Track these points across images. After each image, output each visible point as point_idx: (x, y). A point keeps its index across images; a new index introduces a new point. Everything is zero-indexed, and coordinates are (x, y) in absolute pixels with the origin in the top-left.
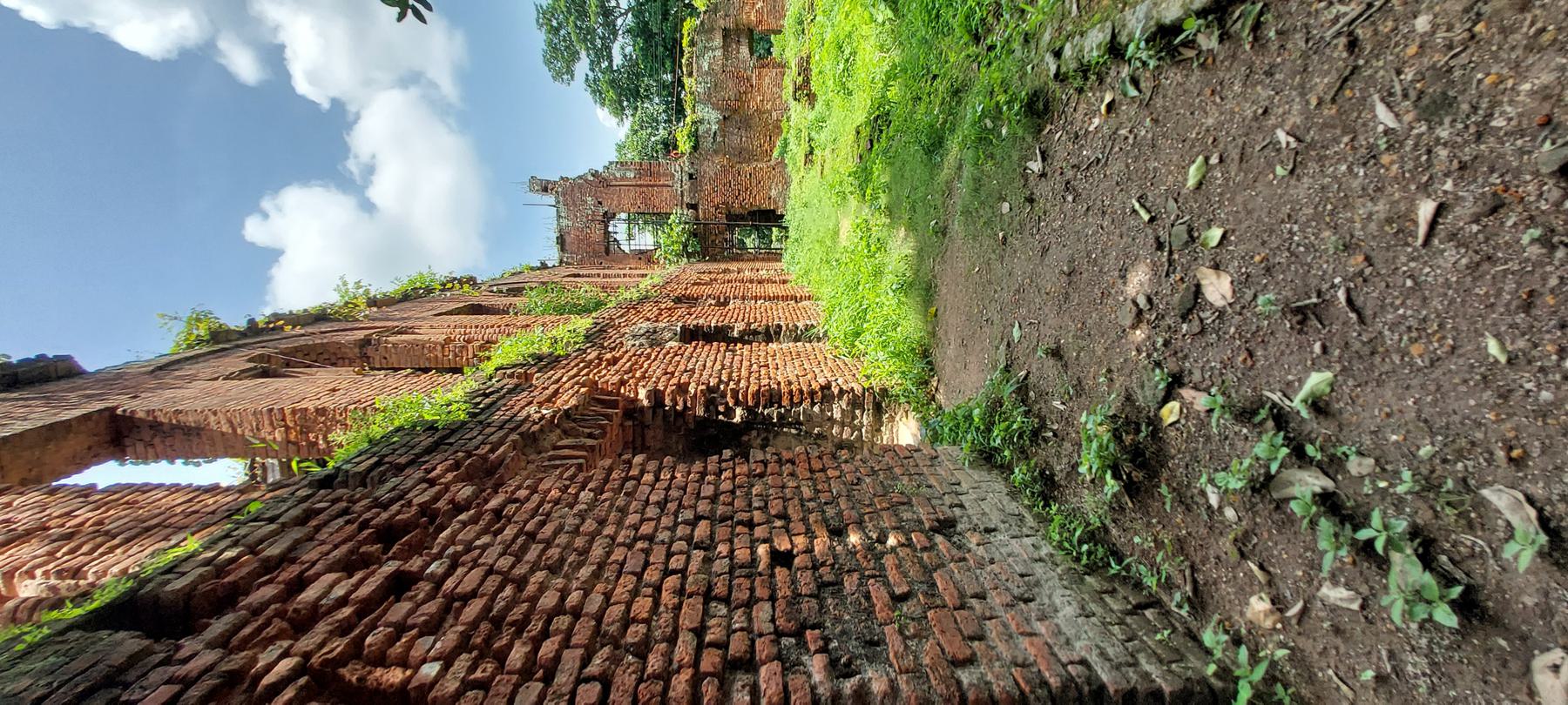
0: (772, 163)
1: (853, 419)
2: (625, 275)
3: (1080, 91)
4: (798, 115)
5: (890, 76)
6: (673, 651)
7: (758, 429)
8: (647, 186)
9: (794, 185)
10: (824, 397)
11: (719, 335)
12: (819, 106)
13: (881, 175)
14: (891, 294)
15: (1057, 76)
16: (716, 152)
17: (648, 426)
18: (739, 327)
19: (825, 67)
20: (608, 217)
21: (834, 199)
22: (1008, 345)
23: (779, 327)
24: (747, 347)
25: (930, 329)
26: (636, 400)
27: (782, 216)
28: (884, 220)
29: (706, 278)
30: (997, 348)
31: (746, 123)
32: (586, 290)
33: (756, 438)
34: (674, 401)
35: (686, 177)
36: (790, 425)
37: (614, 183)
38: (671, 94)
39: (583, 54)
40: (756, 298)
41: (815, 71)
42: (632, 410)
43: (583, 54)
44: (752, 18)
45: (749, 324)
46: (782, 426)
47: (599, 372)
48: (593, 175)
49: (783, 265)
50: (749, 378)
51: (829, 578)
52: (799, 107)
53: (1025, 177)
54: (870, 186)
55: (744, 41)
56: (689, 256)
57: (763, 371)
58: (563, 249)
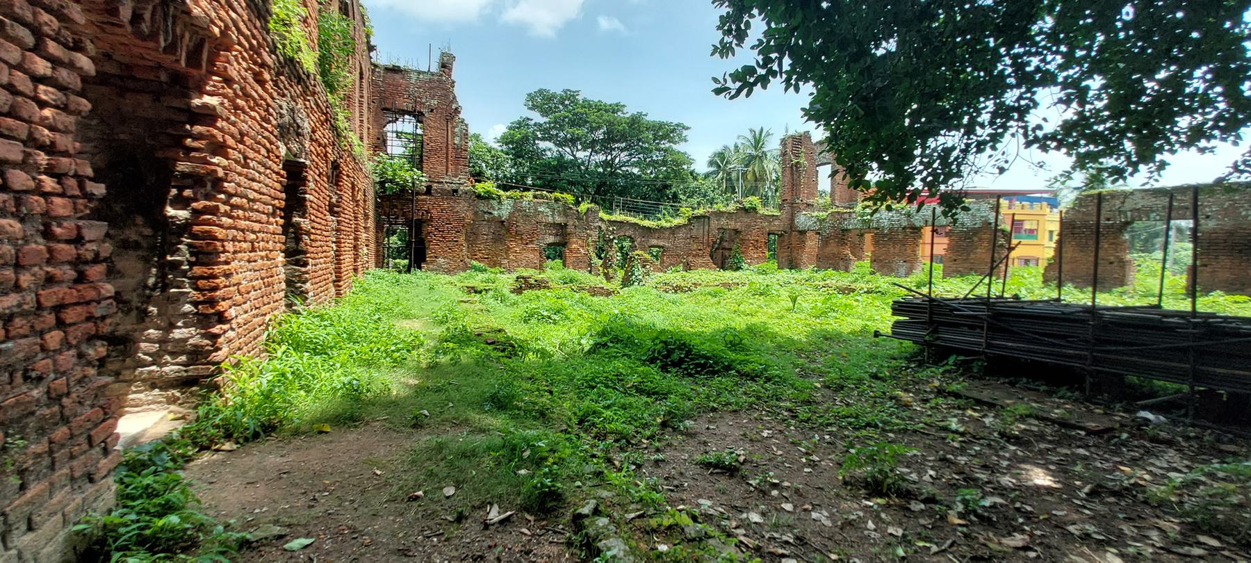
0: (467, 260)
2: (362, 121)
3: (569, 544)
4: (506, 281)
5: (543, 353)
7: (154, 236)
8: (447, 154)
9: (448, 278)
10: (207, 316)
11: (294, 200)
12: (514, 297)
13: (469, 354)
14: (346, 380)
15: (581, 516)
16: (476, 213)
17: (158, 100)
18: (305, 223)
19: (543, 301)
20: (418, 116)
21: (440, 314)
22: (280, 537)
23: (305, 264)
24: (280, 230)
25: (303, 428)
26: (202, 92)
27: (420, 268)
28: (424, 362)
29: (360, 196)
30: (276, 522)
31: (498, 239)
32: (348, 78)
33: (141, 234)
34: (196, 138)
35: (454, 187)
36: (162, 276)
37: (450, 126)
38: (517, 182)
39: (546, 119)
40: (338, 242)
41: (539, 293)
42: (185, 84)
43: (546, 119)
44: (574, 246)
45: (308, 233)
47: (243, 58)
48: (456, 109)
49: (373, 270)
50: (235, 228)
51: (50, 319)
52: (511, 281)
53: (482, 506)
54: (456, 346)
55: (558, 239)
56: (382, 183)
57: (244, 245)
58: (387, 69)
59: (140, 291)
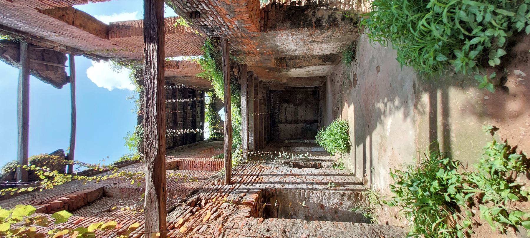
36: (323, 5)
46: (320, 6)
59: (328, 11)
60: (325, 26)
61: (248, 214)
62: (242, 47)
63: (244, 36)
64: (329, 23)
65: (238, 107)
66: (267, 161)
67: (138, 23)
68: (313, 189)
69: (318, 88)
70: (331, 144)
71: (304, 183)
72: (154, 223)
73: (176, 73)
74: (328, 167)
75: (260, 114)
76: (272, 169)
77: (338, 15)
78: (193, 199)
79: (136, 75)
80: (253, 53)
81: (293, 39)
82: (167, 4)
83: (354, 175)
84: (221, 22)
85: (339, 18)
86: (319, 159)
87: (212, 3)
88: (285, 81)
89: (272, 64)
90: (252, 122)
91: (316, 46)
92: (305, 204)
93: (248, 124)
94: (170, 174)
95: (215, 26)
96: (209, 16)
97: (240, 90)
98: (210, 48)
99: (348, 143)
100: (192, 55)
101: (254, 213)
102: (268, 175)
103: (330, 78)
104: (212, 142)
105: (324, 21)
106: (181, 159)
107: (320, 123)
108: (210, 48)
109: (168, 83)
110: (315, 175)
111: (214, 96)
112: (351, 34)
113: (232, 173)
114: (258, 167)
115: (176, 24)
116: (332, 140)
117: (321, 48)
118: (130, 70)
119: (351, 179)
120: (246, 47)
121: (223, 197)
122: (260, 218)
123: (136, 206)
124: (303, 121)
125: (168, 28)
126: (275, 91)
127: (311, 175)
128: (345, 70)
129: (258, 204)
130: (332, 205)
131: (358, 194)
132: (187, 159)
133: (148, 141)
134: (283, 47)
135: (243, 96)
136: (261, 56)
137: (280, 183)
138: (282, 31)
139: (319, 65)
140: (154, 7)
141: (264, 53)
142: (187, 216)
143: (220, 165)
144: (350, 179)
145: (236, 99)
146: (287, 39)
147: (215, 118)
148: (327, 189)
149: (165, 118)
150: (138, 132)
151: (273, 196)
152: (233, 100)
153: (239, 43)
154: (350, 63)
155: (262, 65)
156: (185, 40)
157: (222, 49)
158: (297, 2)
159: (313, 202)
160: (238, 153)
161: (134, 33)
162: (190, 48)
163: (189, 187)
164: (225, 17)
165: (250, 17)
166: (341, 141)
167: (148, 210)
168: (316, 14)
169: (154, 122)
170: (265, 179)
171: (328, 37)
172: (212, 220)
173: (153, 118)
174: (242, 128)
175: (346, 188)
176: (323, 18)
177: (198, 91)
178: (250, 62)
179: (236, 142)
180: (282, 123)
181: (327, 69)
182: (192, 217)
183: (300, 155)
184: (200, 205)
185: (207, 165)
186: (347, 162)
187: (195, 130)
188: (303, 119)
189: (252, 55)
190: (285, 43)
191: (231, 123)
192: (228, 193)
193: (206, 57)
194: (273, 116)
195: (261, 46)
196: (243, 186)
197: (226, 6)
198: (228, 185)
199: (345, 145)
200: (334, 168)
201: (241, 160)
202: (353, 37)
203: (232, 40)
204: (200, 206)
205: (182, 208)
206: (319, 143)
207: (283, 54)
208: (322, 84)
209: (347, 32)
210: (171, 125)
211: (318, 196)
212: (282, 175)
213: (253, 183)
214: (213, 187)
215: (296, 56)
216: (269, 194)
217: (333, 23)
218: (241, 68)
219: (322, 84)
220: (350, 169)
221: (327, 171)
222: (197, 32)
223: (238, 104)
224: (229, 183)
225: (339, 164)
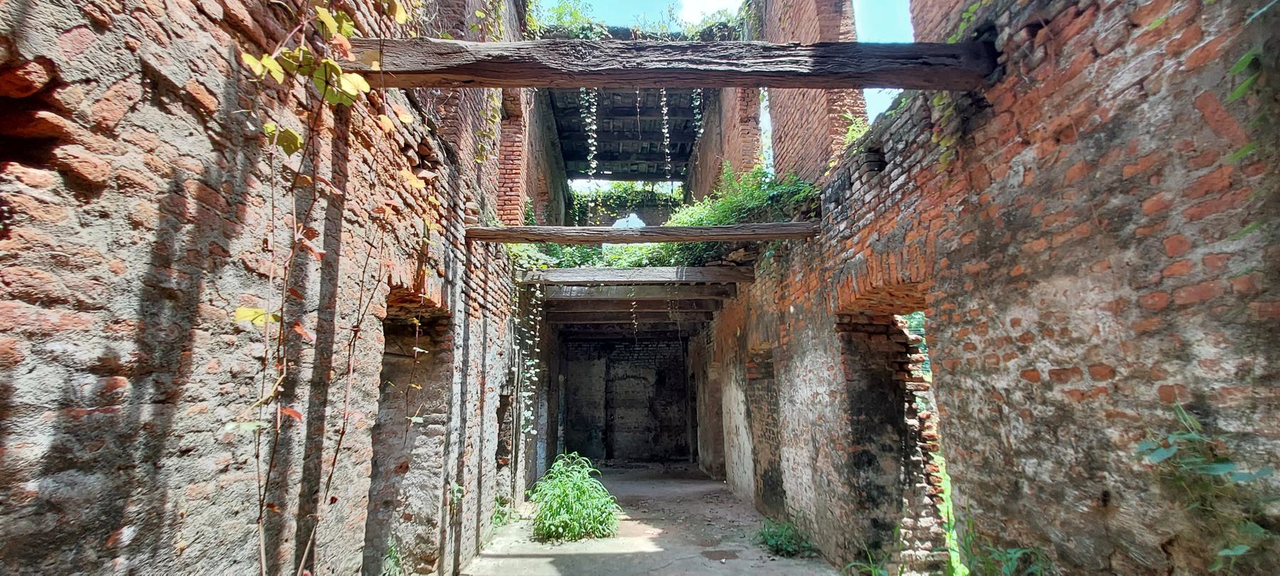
1: (920, 540)
6: (316, 167)
33: (891, 439)
36: (908, 473)
46: (906, 465)
59: (896, 486)
60: (858, 477)
61: (395, 281)
62: (798, 270)
63: (827, 275)
64: (866, 486)
65: (650, 259)
66: (517, 330)
67: (848, 32)
68: (448, 445)
69: (695, 460)
70: (557, 491)
71: (464, 421)
72: (389, 59)
73: (730, 115)
74: (498, 484)
75: (632, 314)
76: (500, 343)
77: (883, 512)
78: (436, 149)
79: (725, 26)
80: (782, 298)
81: (820, 397)
82: (901, 95)
83: (478, 554)
84: (859, 220)
85: (878, 513)
86: (519, 460)
87: (907, 200)
88: (712, 375)
89: (757, 342)
90: (613, 293)
91: (805, 455)
92: (416, 424)
93: (607, 284)
94: (494, 97)
95: (850, 207)
96: (873, 193)
97: (693, 265)
98: (794, 194)
99: (559, 536)
100: (775, 154)
101: (399, 297)
102: (485, 333)
103: (722, 490)
104: (562, 198)
105: (871, 474)
106: (527, 124)
107: (607, 466)
108: (794, 194)
109: (705, 97)
110: (481, 450)
111: (676, 204)
112: (838, 545)
113: (492, 244)
114: (504, 309)
115: (849, 115)
116: (566, 495)
117: (800, 468)
118: (735, 13)
119: (468, 543)
120: (797, 279)
121: (438, 222)
122: (385, 310)
123: (424, 21)
124: (613, 420)
125: (839, 99)
126: (686, 350)
127: (481, 441)
128: (745, 530)
129: (415, 305)
130: (405, 494)
131: (432, 562)
132: (525, 139)
133: (585, 49)
134: (800, 371)
135: (677, 273)
136: (775, 316)
137: (465, 362)
138: (842, 367)
139: (756, 461)
140: (897, 65)
141: (783, 323)
142: (398, 137)
143: (510, 217)
144: (467, 543)
145: (670, 256)
146: (821, 381)
147: (619, 205)
148: (447, 482)
149: (627, 89)
150: (591, 29)
151: (435, 343)
152: (667, 248)
153: (808, 264)
154: (765, 542)
155: (754, 319)
156: (812, 138)
157: (793, 222)
158: (914, 406)
159: (416, 443)
160: (537, 260)
161: (827, 23)
162: (793, 148)
163: (462, 141)
164: (872, 229)
165: (875, 291)
166: (565, 517)
167: (422, 47)
168: (887, 454)
169: (628, 62)
170: (475, 325)
171: (829, 485)
172: (387, 193)
173: (639, 60)
174: (599, 270)
175: (448, 530)
176: (876, 473)
177: (686, 166)
178: (761, 290)
179: (563, 254)
180: (608, 367)
181: (745, 485)
182: (396, 148)
183: (530, 413)
184: (423, 166)
185: (511, 185)
186: (509, 535)
187: (595, 157)
188: (617, 421)
189: (778, 295)
190: (811, 375)
191: (608, 241)
192: (448, 234)
193: (771, 185)
194: (625, 346)
195: (801, 317)
196: (461, 269)
197: (899, 232)
198: (464, 233)
199: (553, 528)
200: (497, 500)
201: (521, 266)
202: (831, 549)
203: (816, 248)
204: (418, 166)
205: (416, 125)
206: (560, 462)
207: (782, 371)
208: (705, 471)
209: (843, 534)
210: (606, 103)
211: (430, 456)
212: (483, 366)
213: (467, 295)
214: (462, 197)
215: (777, 404)
216: (439, 334)
217: (867, 498)
218: (746, 269)
219: (705, 471)
220: (494, 542)
221: (489, 482)
222: (832, 165)
223: (656, 261)
224: (470, 237)
225: (504, 515)
